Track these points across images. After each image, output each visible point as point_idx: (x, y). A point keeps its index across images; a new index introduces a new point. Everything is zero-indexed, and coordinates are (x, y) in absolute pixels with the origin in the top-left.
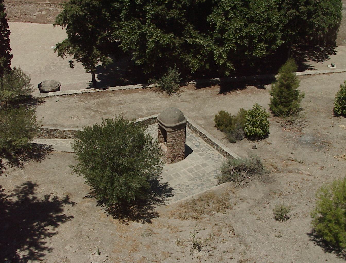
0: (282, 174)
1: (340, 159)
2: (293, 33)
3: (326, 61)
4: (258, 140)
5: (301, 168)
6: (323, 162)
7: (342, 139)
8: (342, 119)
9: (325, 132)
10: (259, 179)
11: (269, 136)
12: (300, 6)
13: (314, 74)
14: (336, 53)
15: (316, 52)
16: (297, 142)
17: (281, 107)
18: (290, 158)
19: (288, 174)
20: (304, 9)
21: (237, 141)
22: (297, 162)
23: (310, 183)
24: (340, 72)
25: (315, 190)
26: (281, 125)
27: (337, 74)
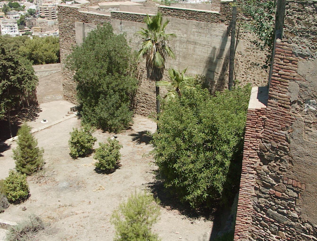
0: (61, 222)
1: (99, 190)
2: (10, 101)
3: (37, 118)
4: (23, 201)
5: (73, 210)
6: (88, 198)
7: (90, 175)
8: (81, 160)
9: (74, 175)
10: (44, 233)
11: (30, 194)
12: (10, 76)
13: (37, 131)
14: (41, 110)
15: (24, 114)
16: (57, 190)
17: (28, 166)
18: (60, 205)
19: (66, 219)
20: (15, 78)
21: (5, 210)
22: (67, 207)
23: (88, 219)
24: (57, 124)
25: (95, 222)
26: (35, 182)
27: (55, 126)
